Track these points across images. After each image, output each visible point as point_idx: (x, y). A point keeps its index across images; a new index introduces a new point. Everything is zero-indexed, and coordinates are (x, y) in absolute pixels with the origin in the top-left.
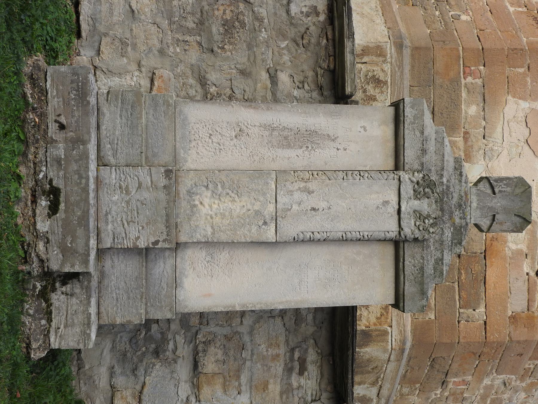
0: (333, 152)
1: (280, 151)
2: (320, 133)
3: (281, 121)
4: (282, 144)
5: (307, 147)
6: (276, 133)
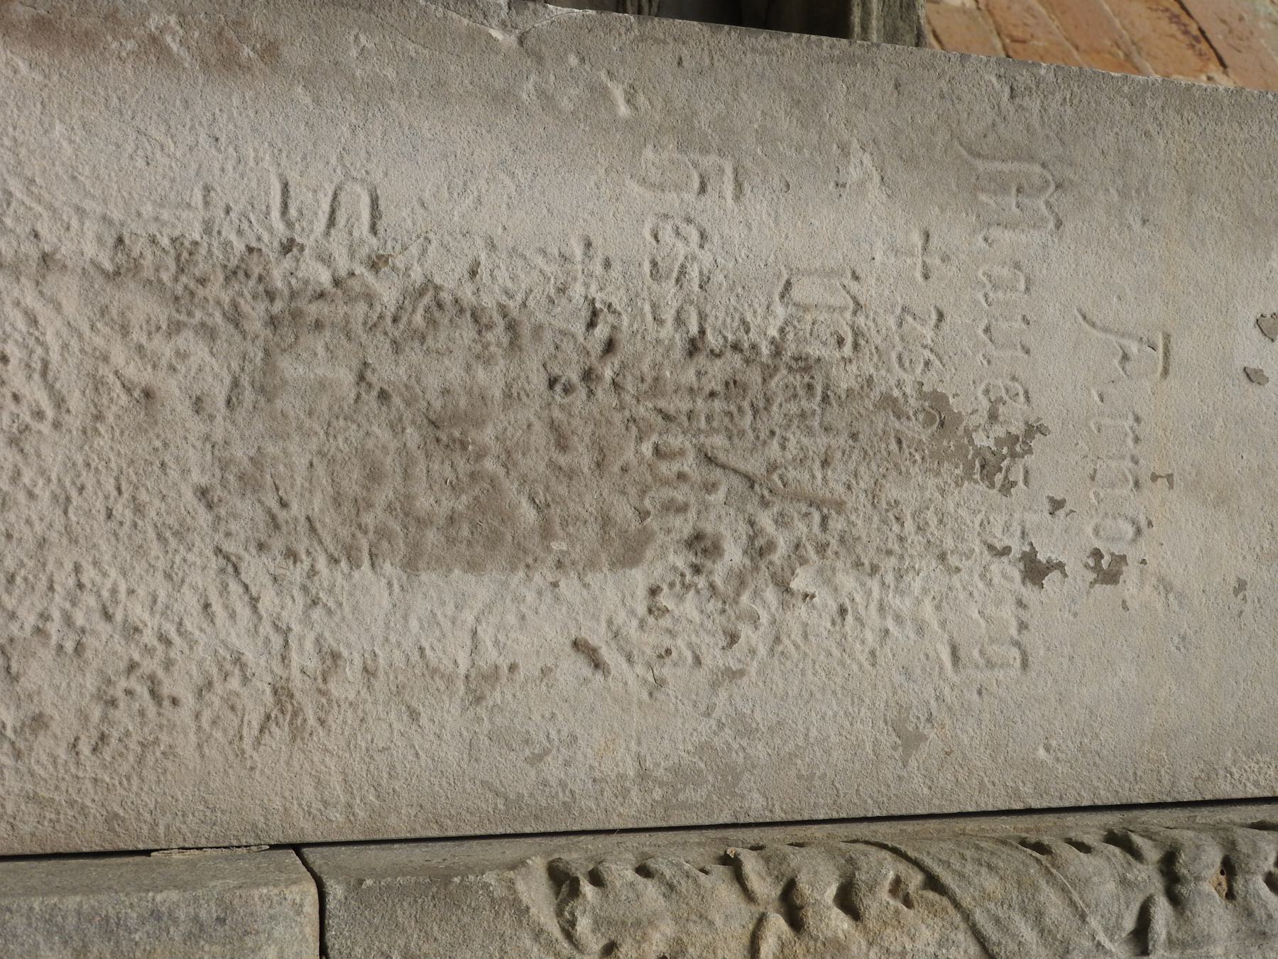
0: (986, 599)
1: (374, 588)
2: (845, 380)
3: (396, 216)
4: (404, 508)
5: (702, 546)
6: (316, 366)
